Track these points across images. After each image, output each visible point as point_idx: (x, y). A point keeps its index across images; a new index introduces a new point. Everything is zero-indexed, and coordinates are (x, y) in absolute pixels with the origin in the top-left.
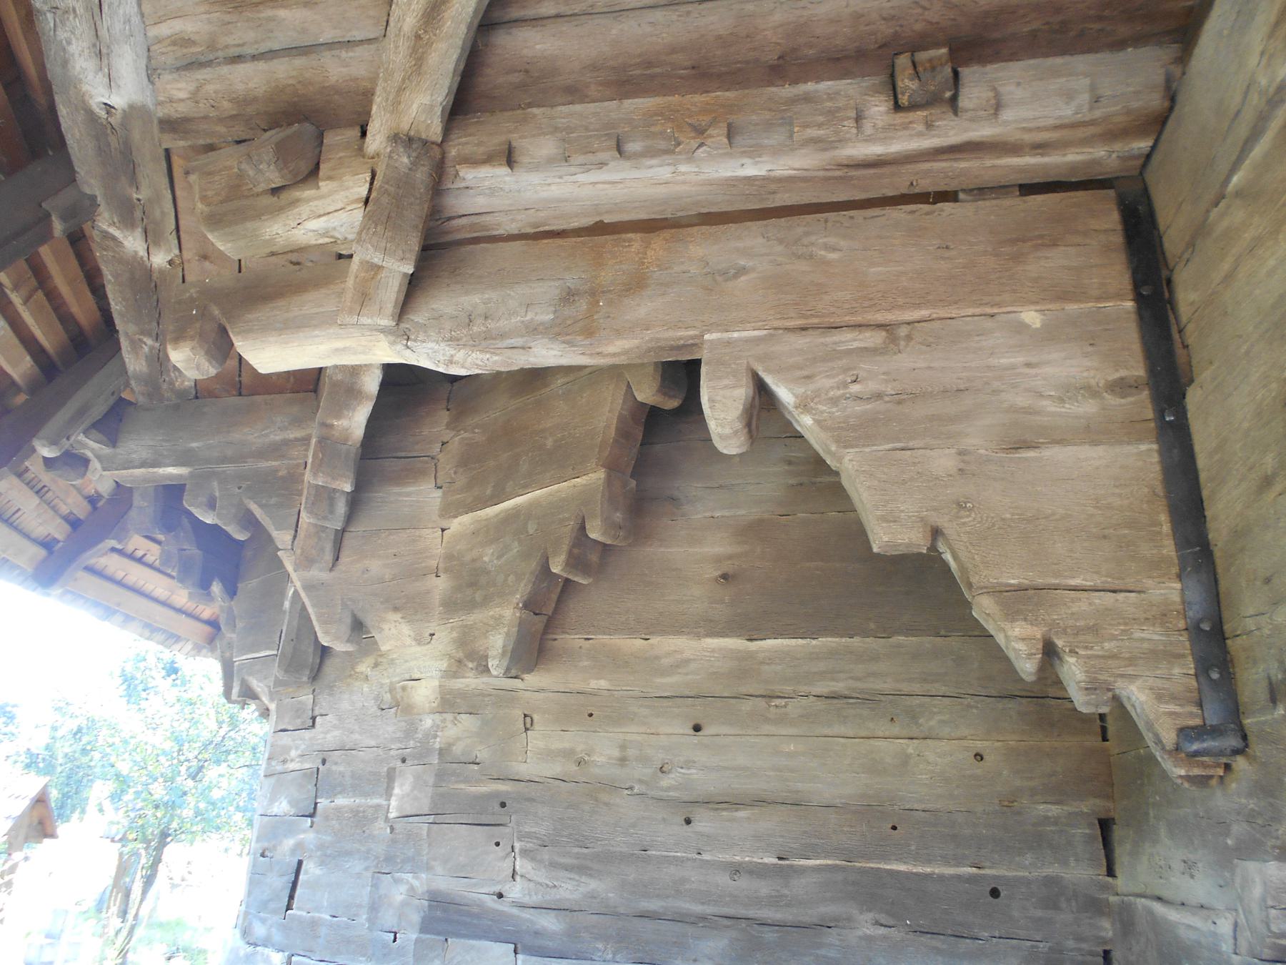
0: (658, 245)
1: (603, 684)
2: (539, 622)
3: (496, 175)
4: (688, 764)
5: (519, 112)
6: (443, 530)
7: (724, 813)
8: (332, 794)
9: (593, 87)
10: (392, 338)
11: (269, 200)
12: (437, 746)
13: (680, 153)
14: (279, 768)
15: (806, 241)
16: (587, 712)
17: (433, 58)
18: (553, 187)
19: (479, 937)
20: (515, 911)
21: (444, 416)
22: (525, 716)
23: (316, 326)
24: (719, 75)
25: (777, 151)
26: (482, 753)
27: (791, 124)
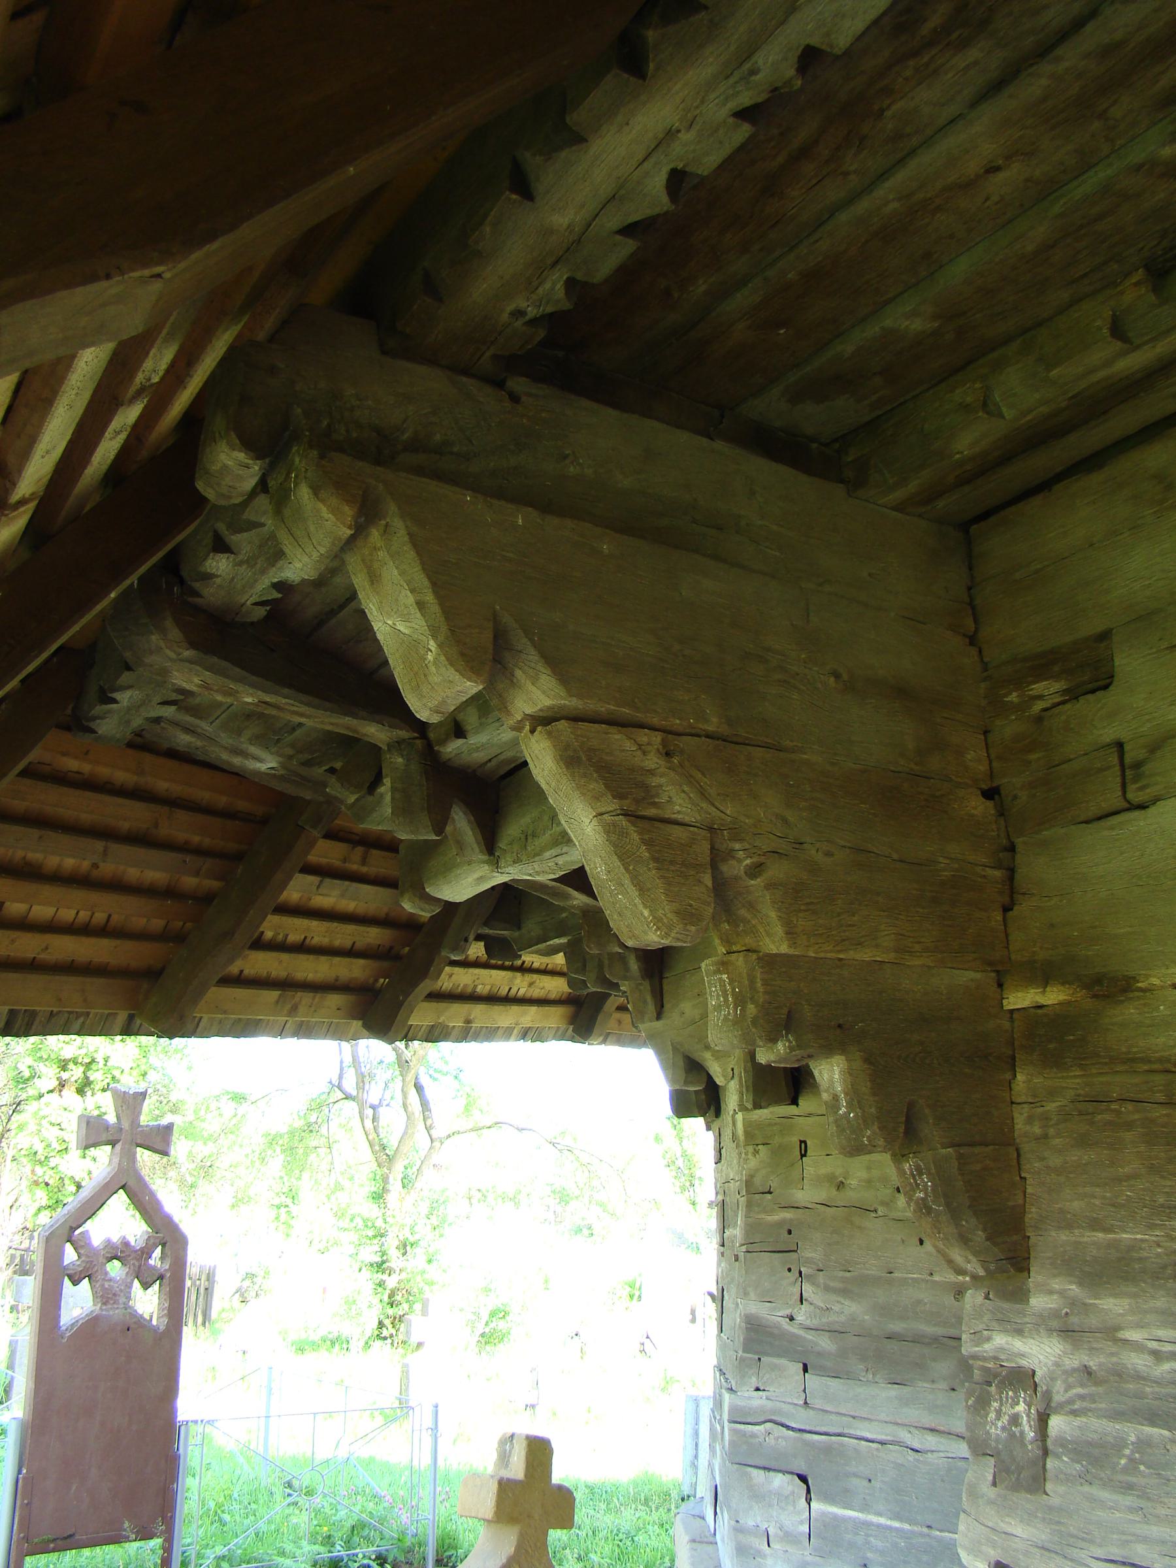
19: (779, 1356)
20: (801, 1333)
26: (774, 1183)
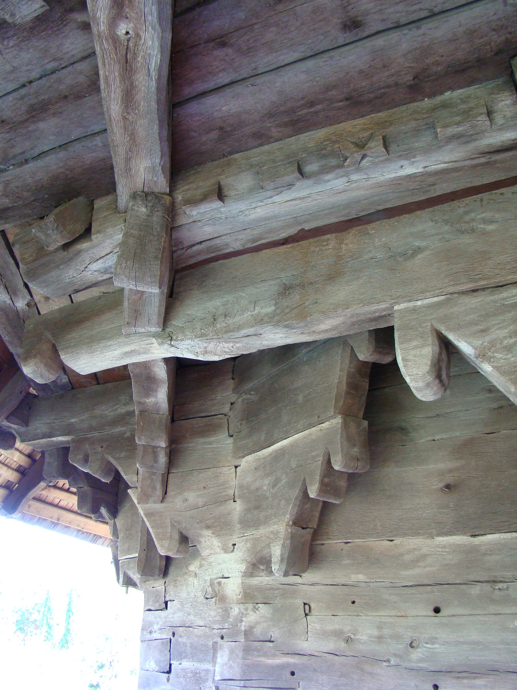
0: (351, 240)
1: (361, 577)
2: (307, 534)
3: (211, 208)
4: (432, 640)
5: (225, 159)
6: (236, 467)
7: (465, 681)
8: (181, 656)
9: (274, 130)
10: (160, 340)
11: (62, 254)
12: (243, 628)
13: (349, 166)
14: (148, 637)
15: (467, 218)
16: (352, 601)
17: (141, 132)
18: (258, 210)
21: (231, 383)
22: (305, 604)
23: (110, 339)
24: (370, 101)
25: (427, 151)
26: (275, 633)
27: (434, 128)
